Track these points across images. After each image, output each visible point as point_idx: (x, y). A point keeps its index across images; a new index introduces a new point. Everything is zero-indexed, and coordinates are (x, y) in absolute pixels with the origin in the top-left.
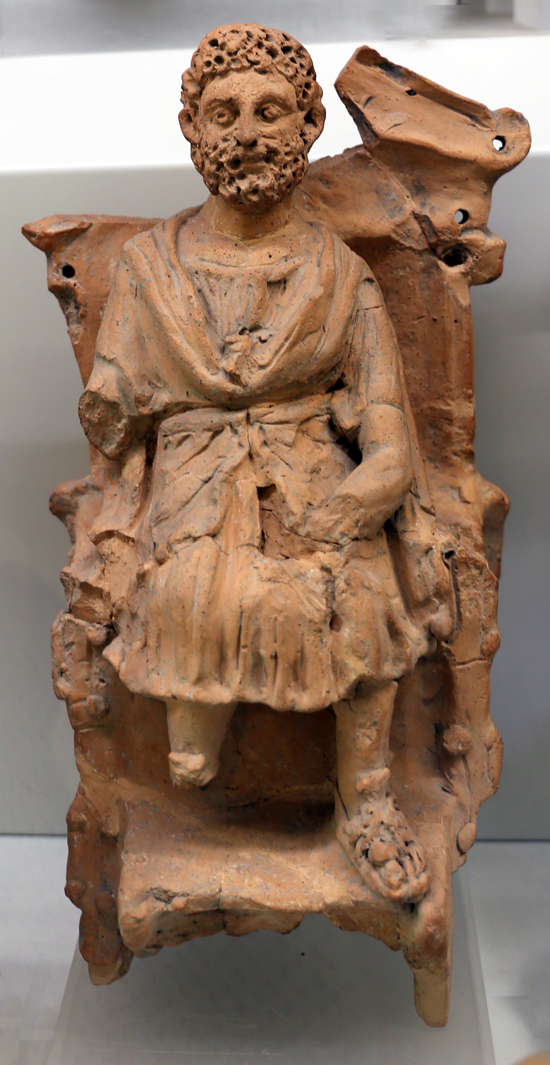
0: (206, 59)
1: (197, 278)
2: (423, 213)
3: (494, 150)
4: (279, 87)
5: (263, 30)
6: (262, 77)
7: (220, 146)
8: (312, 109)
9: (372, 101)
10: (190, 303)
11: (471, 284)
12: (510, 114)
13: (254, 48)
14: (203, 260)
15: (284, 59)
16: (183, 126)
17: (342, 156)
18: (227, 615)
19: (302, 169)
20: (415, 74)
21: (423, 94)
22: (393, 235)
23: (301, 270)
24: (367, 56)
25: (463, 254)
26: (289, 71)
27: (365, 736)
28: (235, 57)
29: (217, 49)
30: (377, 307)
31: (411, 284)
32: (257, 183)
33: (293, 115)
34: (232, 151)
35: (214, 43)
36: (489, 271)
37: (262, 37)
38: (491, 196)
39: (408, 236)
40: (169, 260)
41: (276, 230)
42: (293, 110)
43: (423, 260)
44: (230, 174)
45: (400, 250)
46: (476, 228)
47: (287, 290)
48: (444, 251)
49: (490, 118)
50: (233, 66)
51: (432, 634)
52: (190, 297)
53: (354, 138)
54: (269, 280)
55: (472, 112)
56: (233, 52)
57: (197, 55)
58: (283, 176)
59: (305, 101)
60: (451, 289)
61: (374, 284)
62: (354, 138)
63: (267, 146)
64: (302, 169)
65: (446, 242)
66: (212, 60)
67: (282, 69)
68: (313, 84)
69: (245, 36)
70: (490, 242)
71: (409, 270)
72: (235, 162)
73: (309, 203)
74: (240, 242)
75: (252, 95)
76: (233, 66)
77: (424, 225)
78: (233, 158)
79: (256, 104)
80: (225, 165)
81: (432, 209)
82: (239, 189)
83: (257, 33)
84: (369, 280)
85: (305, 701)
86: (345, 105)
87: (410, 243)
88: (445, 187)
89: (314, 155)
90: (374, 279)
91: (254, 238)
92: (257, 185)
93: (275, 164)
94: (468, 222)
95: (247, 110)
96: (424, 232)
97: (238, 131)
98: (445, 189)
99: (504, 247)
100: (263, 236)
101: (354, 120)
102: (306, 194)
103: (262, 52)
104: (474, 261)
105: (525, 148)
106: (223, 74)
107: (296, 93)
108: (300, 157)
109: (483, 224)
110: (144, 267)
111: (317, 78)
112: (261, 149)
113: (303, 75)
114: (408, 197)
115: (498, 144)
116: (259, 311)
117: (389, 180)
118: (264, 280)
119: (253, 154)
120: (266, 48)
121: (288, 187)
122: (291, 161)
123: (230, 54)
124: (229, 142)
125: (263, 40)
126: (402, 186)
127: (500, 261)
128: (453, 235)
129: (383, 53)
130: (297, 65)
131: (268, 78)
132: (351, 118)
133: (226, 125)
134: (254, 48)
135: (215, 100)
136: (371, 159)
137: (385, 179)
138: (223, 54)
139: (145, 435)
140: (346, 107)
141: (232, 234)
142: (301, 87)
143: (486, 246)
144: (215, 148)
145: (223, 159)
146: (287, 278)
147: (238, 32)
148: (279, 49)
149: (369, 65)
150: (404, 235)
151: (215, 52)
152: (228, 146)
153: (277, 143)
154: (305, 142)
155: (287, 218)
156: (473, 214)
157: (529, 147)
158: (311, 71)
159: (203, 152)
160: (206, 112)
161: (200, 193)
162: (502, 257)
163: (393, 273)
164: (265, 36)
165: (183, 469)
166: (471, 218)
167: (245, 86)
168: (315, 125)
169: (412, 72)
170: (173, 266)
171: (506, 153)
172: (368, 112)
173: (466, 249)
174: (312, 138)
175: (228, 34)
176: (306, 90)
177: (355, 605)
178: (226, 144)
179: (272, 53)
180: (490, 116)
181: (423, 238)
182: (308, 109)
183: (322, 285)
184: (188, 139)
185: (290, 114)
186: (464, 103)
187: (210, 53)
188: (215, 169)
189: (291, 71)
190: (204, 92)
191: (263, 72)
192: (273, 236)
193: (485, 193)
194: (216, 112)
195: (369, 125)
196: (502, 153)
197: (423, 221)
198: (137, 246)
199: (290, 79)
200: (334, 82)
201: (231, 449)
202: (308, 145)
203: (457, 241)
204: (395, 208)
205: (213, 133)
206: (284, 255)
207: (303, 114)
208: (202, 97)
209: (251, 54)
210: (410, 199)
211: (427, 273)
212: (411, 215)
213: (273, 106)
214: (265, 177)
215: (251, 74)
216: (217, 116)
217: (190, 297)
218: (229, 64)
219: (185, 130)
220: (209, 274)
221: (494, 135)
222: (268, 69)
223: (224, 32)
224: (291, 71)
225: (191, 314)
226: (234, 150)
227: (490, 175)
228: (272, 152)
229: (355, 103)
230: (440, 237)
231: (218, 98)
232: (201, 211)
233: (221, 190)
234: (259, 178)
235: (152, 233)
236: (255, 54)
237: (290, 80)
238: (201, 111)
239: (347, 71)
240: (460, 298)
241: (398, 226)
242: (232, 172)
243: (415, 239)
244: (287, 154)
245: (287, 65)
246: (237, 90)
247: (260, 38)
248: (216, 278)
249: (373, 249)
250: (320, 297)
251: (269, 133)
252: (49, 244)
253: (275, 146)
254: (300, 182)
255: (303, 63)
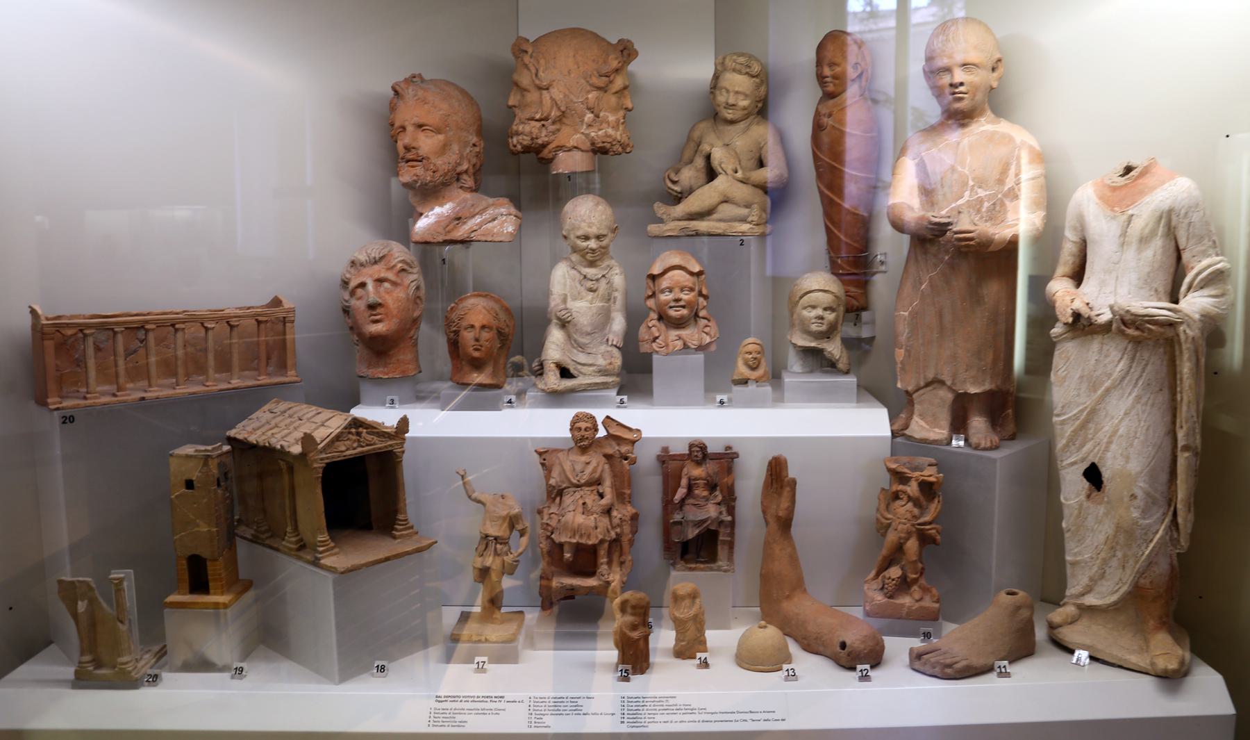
4: (589, 425)
18: (576, 525)
24: (608, 417)
27: (602, 552)
36: (634, 462)
51: (617, 534)
53: (605, 433)
55: (630, 429)
62: (605, 433)
85: (590, 543)
139: (560, 493)
161: (572, 444)
165: (568, 500)
167: (583, 425)
177: (600, 524)
188: (577, 440)
201: (578, 495)
227: (633, 442)
249: (608, 457)
251: (587, 434)
252: (540, 454)
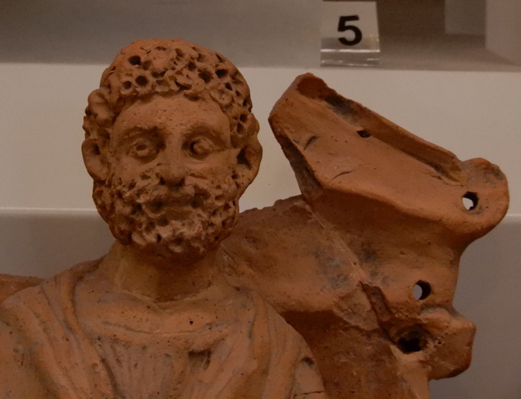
0: (125, 79)
1: (100, 346)
2: (374, 285)
3: (464, 210)
4: (213, 117)
5: (194, 48)
6: (194, 104)
7: (137, 184)
8: (246, 147)
9: (316, 142)
10: (96, 373)
11: (432, 376)
12: (484, 166)
13: (184, 70)
14: (107, 323)
15: (219, 84)
16: (87, 158)
17: (273, 209)
19: (233, 218)
20: (370, 111)
21: (378, 136)
22: (336, 310)
23: (229, 341)
25: (423, 338)
26: (224, 99)
28: (161, 79)
29: (139, 68)
30: (319, 392)
31: (355, 374)
32: (181, 231)
33: (226, 152)
34: (153, 190)
35: (135, 60)
37: (194, 57)
38: (458, 266)
39: (354, 313)
40: (66, 322)
41: (198, 292)
42: (227, 145)
43: (372, 344)
44: (148, 218)
45: (343, 330)
46: (439, 306)
47: (211, 364)
48: (399, 333)
49: (459, 170)
50: (158, 89)
52: (95, 365)
53: (291, 187)
54: (191, 350)
56: (159, 72)
57: (111, 74)
58: (212, 224)
59: (240, 136)
60: (405, 381)
61: (314, 366)
62: (291, 187)
63: (196, 187)
64: (233, 218)
65: (400, 320)
66: (132, 80)
67: (217, 96)
68: (249, 117)
69: (174, 54)
70: (456, 324)
71: (353, 356)
72: (157, 204)
73: (230, 266)
74: (154, 305)
75: (181, 124)
76: (158, 89)
77: (374, 300)
78: (155, 199)
79: (185, 135)
80: (144, 207)
81: (384, 280)
82: (159, 237)
83: (189, 52)
84: (308, 360)
86: (281, 145)
87: (356, 322)
88: (402, 253)
89: (246, 203)
90: (314, 360)
91: (172, 300)
92: (181, 234)
93: (204, 209)
94: (430, 297)
95: (175, 142)
96: (373, 308)
97: (163, 167)
98: (402, 256)
99: (473, 331)
100: (182, 298)
101: (292, 164)
102: (228, 254)
103: (194, 74)
104: (435, 347)
105: (502, 208)
106: (146, 98)
107: (230, 126)
108: (231, 204)
109: (448, 301)
110: (34, 327)
111: (252, 109)
112: (189, 190)
113: (239, 105)
114: (355, 264)
115: (468, 203)
116: (179, 386)
117: (332, 241)
118: (186, 349)
119: (180, 195)
120: (199, 70)
121: (216, 238)
122: (221, 206)
123: (155, 74)
124: (149, 180)
125: (196, 61)
126: (349, 249)
127: (468, 348)
128: (410, 313)
129: (331, 84)
130: (233, 93)
131: (199, 106)
132: (287, 162)
133: (145, 159)
134: (184, 70)
135: (135, 128)
136: (310, 213)
137: (327, 240)
138: (147, 74)
140: (282, 148)
141: (143, 294)
142: (235, 118)
143: (451, 328)
144: (132, 186)
145: (141, 200)
146: (212, 349)
147: (164, 49)
148: (213, 71)
149: (313, 98)
150: (350, 310)
151: (137, 71)
152: (149, 184)
153: (207, 184)
154: (238, 186)
155: (210, 278)
156: (436, 288)
157: (507, 208)
158: (247, 102)
159: (114, 191)
160: (121, 144)
162: (470, 344)
163: (334, 359)
164: (198, 56)
166: (433, 293)
167: (174, 115)
168: (249, 166)
169: (366, 108)
170: (70, 329)
171: (478, 213)
172: (310, 156)
173: (428, 332)
174: (246, 182)
175: (152, 51)
176: (241, 123)
178: (145, 183)
179: (205, 76)
180: (460, 167)
181: (373, 315)
182: (242, 145)
183: (255, 359)
184: (92, 175)
185: (223, 150)
186: (429, 150)
187: (130, 73)
189: (226, 99)
190: (119, 119)
191: (194, 98)
192: (194, 299)
193: (451, 263)
194: (135, 143)
195: (310, 173)
196: (473, 214)
197: (374, 294)
198: (25, 303)
199: (225, 108)
200: (267, 116)
202: (240, 189)
203: (414, 319)
204: (338, 276)
205: (129, 168)
206: (208, 321)
207: (237, 151)
208: (116, 124)
209: (180, 76)
210: (358, 266)
211: (377, 361)
212: (358, 285)
213: (205, 140)
214: (191, 224)
215: (180, 99)
216: (135, 148)
217: (95, 365)
218: (153, 87)
219: (89, 164)
220: (115, 340)
221: (464, 191)
222: (200, 95)
223: (148, 48)
224: (226, 99)
225: (96, 386)
226: (155, 188)
227: (458, 240)
228: (201, 194)
229: (294, 142)
230: (394, 314)
231: (140, 126)
232: (100, 266)
233: (136, 238)
234: (184, 225)
235: (42, 289)
236: (185, 76)
237: (225, 110)
238: (114, 142)
239: (285, 102)
240: (416, 393)
241: (342, 298)
242: (152, 215)
243: (362, 315)
244: (217, 198)
245: (222, 92)
246: (163, 118)
247: (192, 58)
248: (124, 345)
249: (313, 325)
250: (254, 372)
251: (203, 171)
253: (206, 187)
254: (229, 234)
255: (240, 91)
